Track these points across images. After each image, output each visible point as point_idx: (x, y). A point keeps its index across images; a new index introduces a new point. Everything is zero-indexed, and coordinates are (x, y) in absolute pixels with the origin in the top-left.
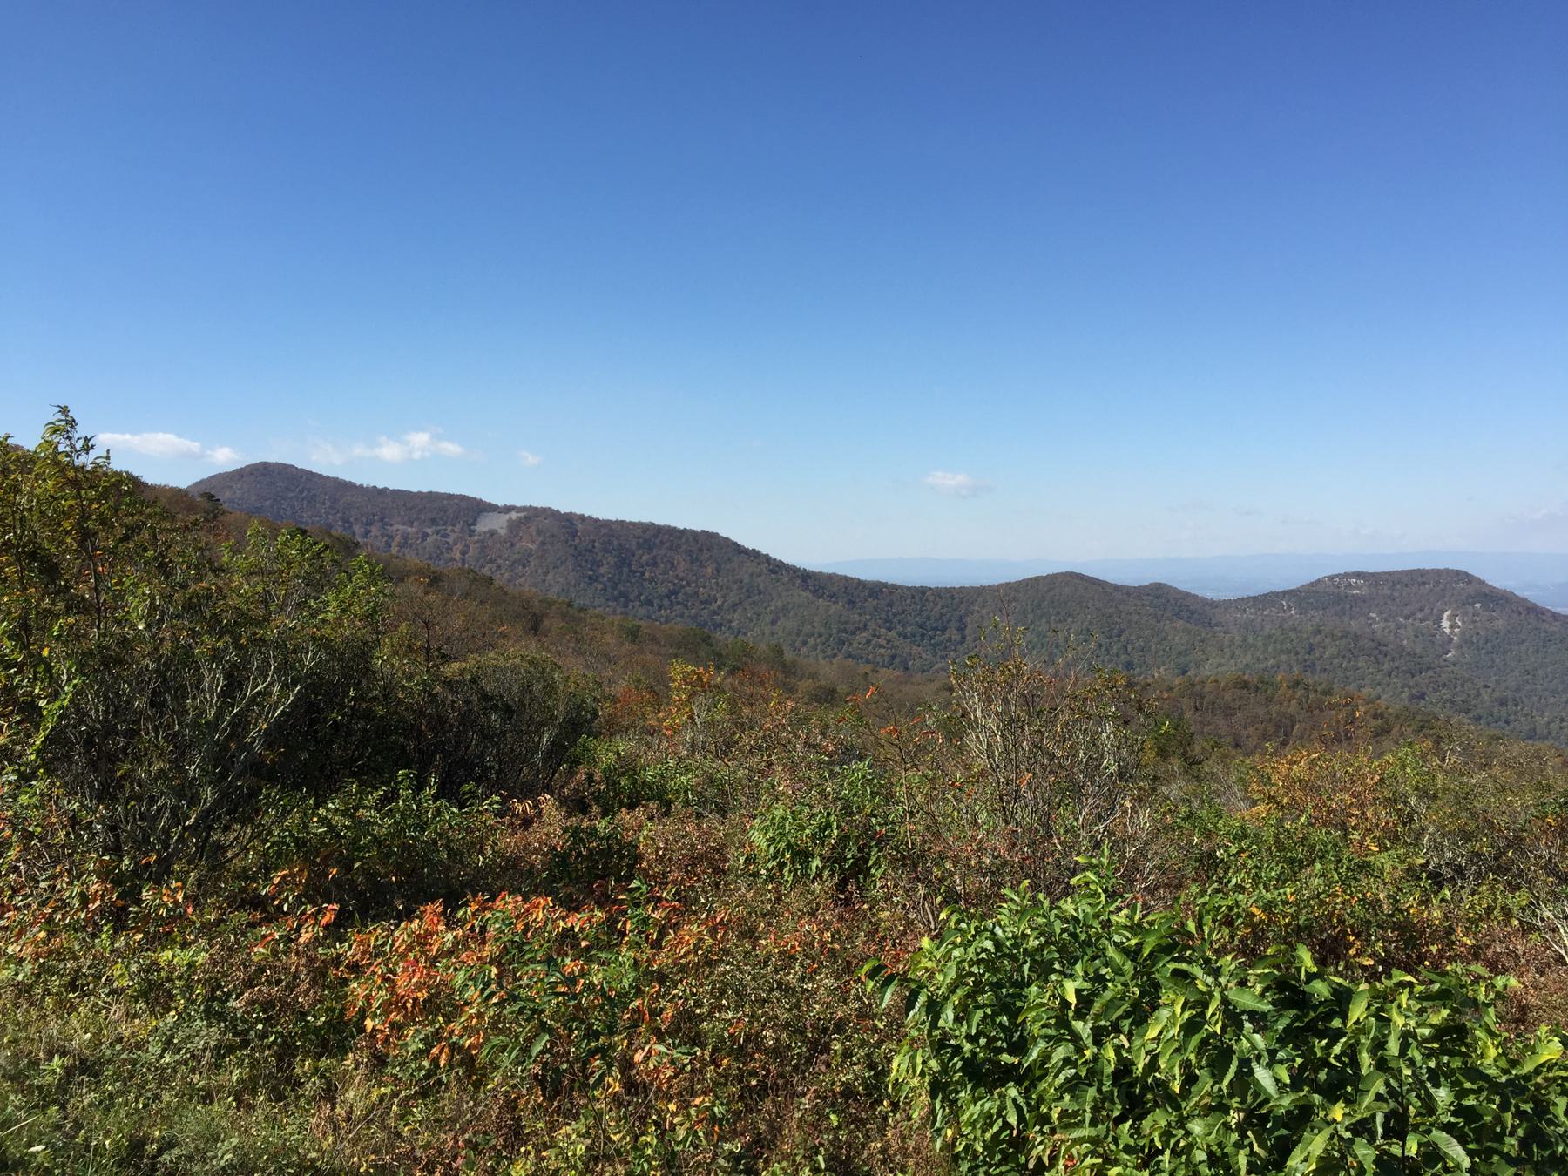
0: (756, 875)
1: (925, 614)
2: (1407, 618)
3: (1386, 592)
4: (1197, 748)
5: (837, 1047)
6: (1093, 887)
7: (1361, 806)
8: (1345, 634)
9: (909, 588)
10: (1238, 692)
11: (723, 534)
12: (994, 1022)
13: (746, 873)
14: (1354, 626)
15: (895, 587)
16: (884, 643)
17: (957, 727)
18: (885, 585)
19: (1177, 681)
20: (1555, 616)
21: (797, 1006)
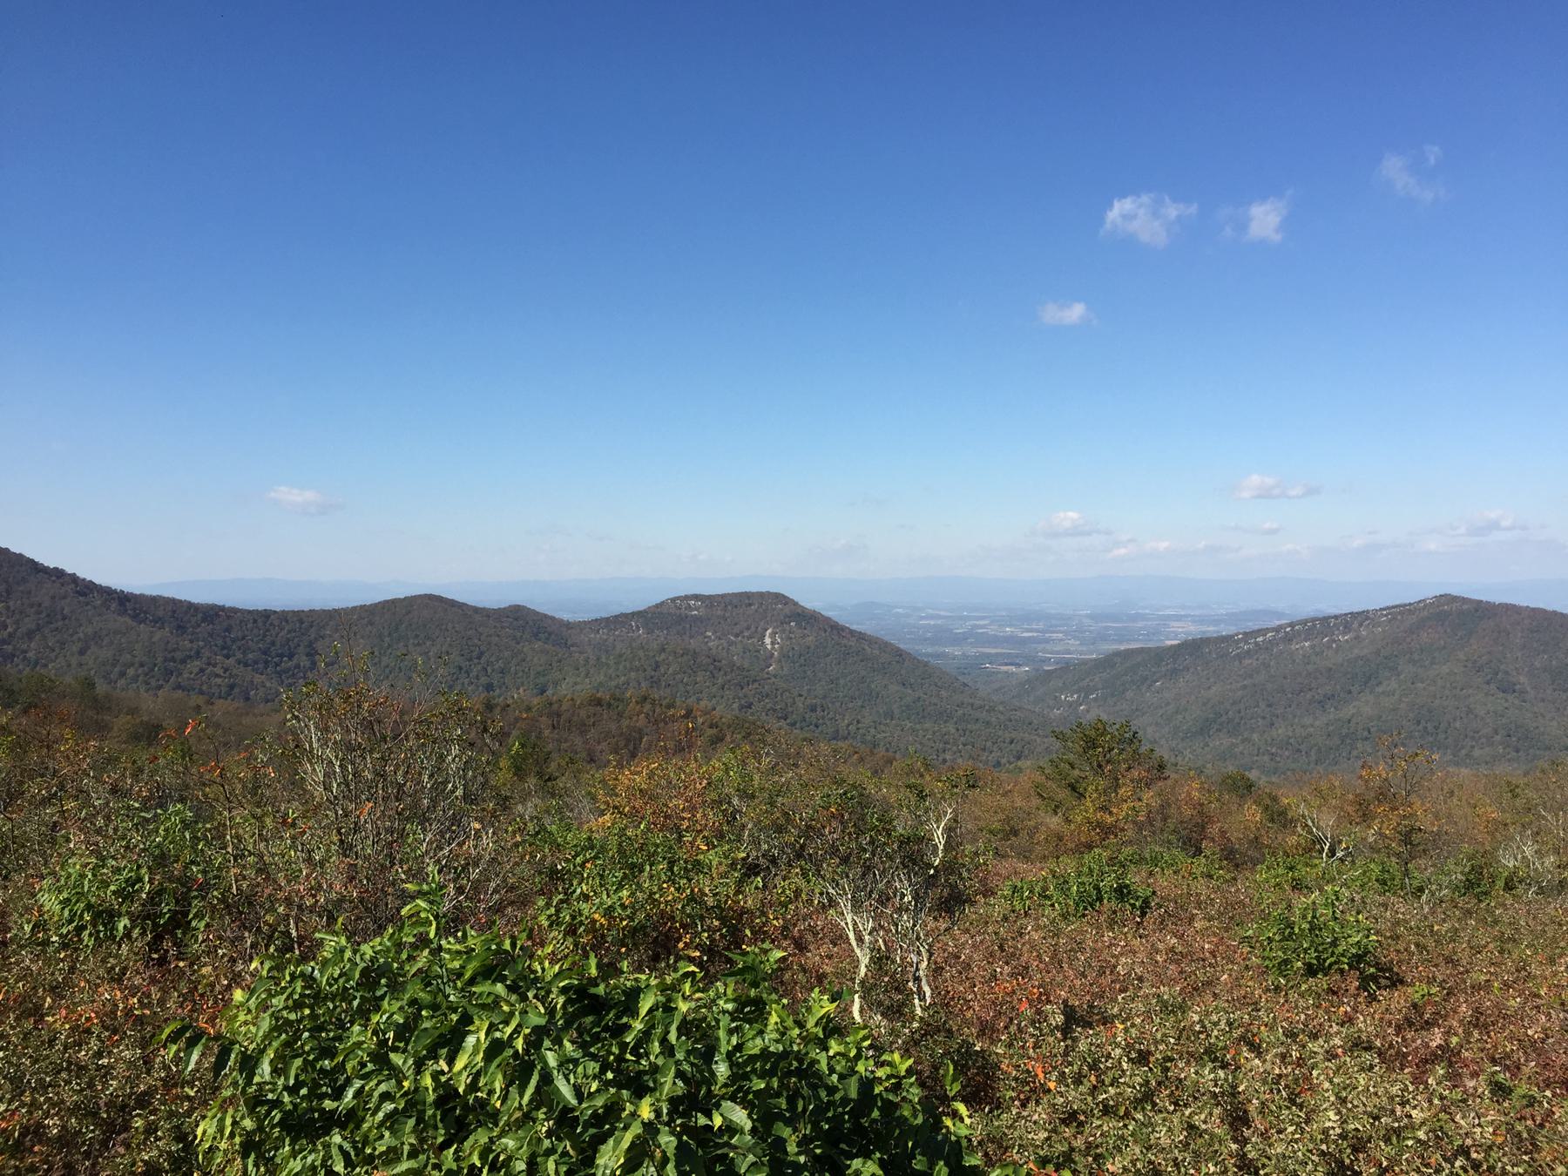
0: (46, 943)
1: (268, 639)
2: (737, 636)
4: (553, 765)
5: (139, 1123)
6: (423, 915)
7: (693, 809)
9: (249, 612)
10: (592, 709)
11: (15, 549)
12: (314, 1068)
13: (32, 941)
14: (694, 644)
15: (235, 610)
16: (221, 672)
17: (293, 754)
18: (222, 608)
19: (535, 701)
20: (852, 632)
21: (91, 1085)
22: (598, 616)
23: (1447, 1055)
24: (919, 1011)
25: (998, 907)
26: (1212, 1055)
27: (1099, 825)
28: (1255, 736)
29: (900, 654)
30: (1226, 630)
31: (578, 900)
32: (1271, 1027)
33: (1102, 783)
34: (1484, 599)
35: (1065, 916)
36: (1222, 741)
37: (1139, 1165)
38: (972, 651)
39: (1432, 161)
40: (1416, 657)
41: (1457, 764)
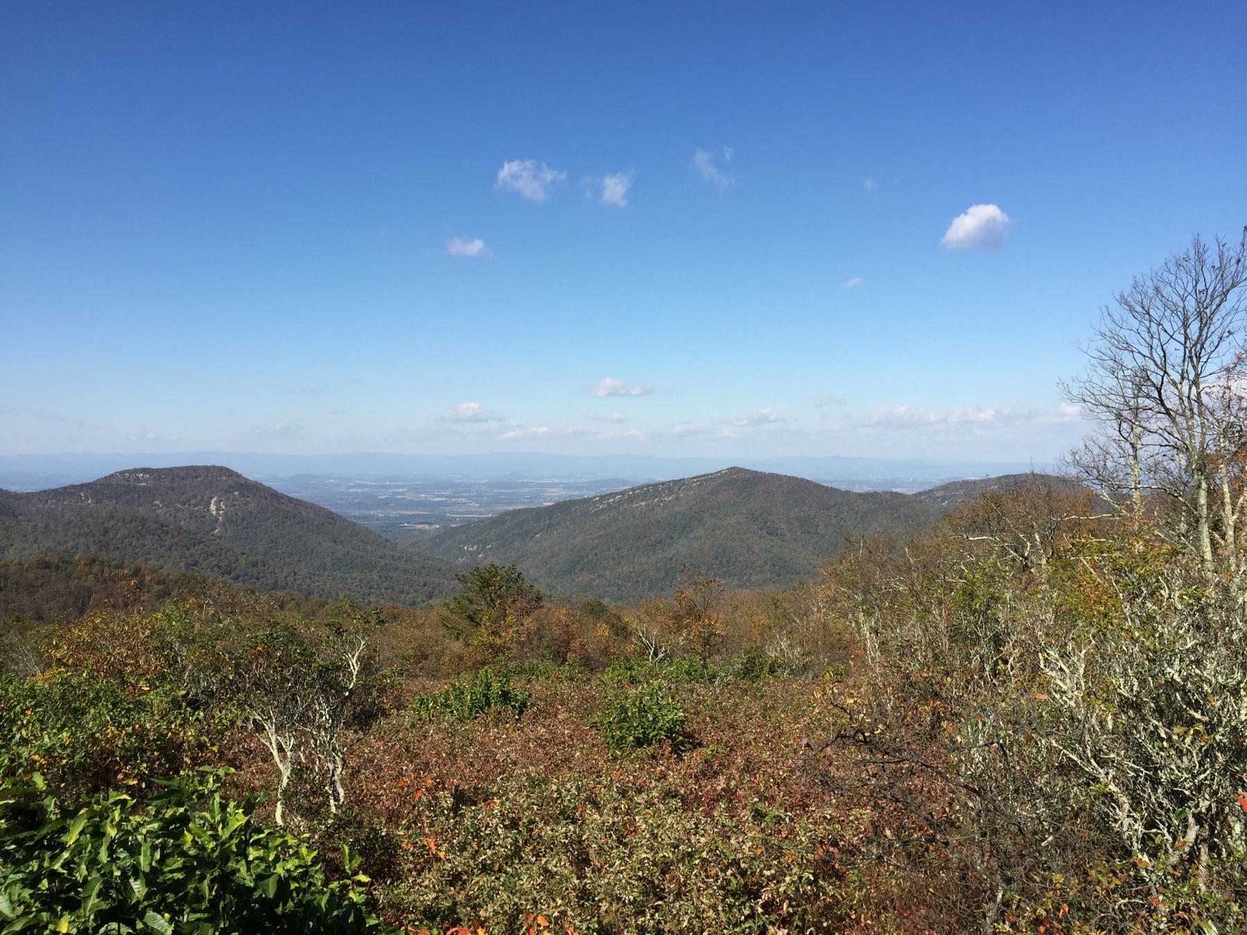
2: (184, 504)
3: (167, 484)
8: (134, 519)
10: (41, 572)
14: (142, 511)
20: (290, 500)
22: (47, 487)
23: (729, 794)
24: (333, 810)
25: (407, 718)
26: (567, 816)
27: (491, 646)
28: (607, 572)
29: (332, 517)
30: (587, 494)
31: (18, 744)
32: (608, 788)
33: (494, 613)
34: (759, 470)
35: (461, 720)
36: (584, 578)
37: (506, 908)
38: (393, 513)
39: (728, 159)
40: (715, 511)
41: (741, 587)
